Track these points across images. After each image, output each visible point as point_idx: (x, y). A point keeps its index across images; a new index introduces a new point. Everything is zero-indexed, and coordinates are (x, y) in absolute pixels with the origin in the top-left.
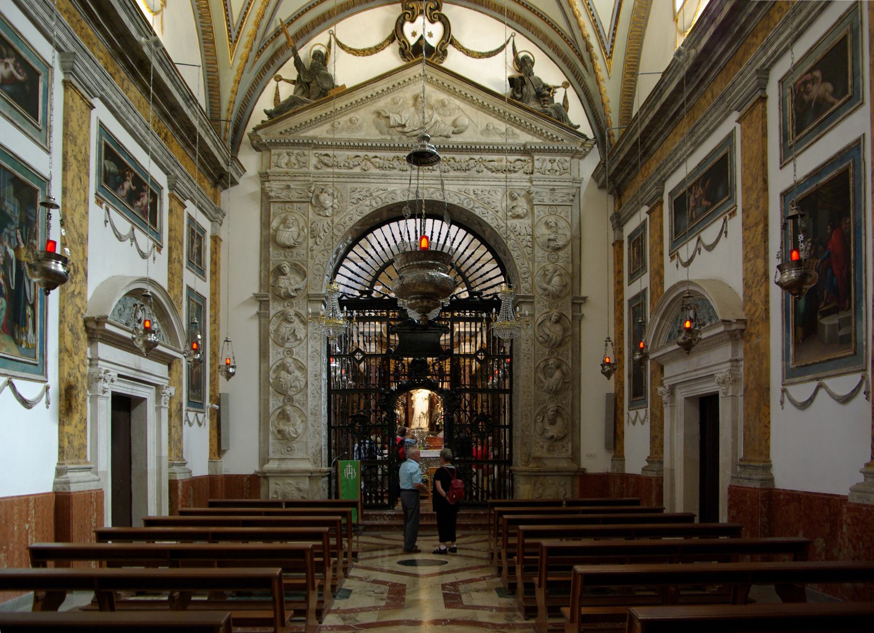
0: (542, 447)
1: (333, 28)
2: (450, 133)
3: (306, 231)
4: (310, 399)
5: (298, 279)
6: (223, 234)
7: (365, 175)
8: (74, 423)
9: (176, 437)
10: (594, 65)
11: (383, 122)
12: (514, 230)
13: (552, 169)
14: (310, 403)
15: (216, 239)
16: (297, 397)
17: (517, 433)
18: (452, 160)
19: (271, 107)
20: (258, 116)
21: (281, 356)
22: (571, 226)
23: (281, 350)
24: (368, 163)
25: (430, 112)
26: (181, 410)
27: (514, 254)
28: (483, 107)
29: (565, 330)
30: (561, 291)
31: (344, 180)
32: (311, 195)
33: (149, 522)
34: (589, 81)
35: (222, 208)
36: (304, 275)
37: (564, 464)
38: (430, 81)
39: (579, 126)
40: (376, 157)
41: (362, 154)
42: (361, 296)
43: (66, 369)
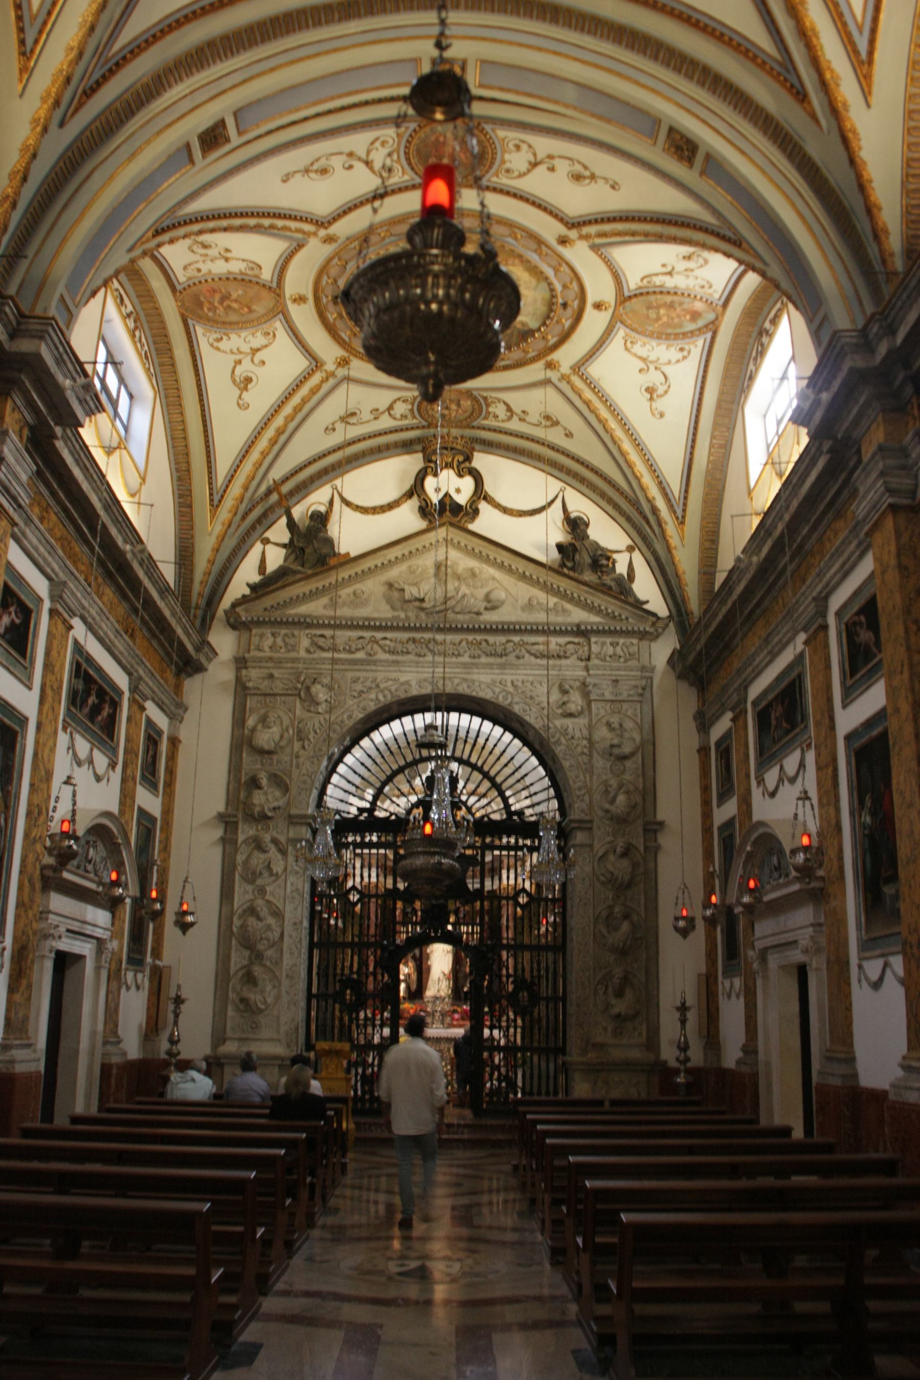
0: (605, 1029)
1: (338, 482)
2: (482, 610)
3: (291, 732)
4: (286, 956)
5: (278, 794)
6: (184, 733)
7: (370, 661)
8: (21, 990)
9: (112, 1005)
10: (663, 532)
11: (396, 594)
12: (565, 732)
13: (615, 654)
14: (285, 962)
15: (174, 742)
16: (269, 953)
17: (571, 1009)
18: (484, 644)
19: (256, 578)
20: (238, 586)
21: (250, 896)
22: (641, 728)
23: (250, 888)
24: (376, 647)
25: (457, 584)
26: (120, 969)
27: (566, 764)
28: (523, 577)
29: (635, 865)
30: (629, 814)
31: (344, 667)
32: (299, 686)
33: (75, 1120)
34: (659, 547)
35: (185, 701)
36: (286, 789)
37: (635, 1054)
38: (458, 546)
39: (647, 602)
40: (385, 638)
41: (367, 634)
42: (360, 814)
43: (22, 925)
